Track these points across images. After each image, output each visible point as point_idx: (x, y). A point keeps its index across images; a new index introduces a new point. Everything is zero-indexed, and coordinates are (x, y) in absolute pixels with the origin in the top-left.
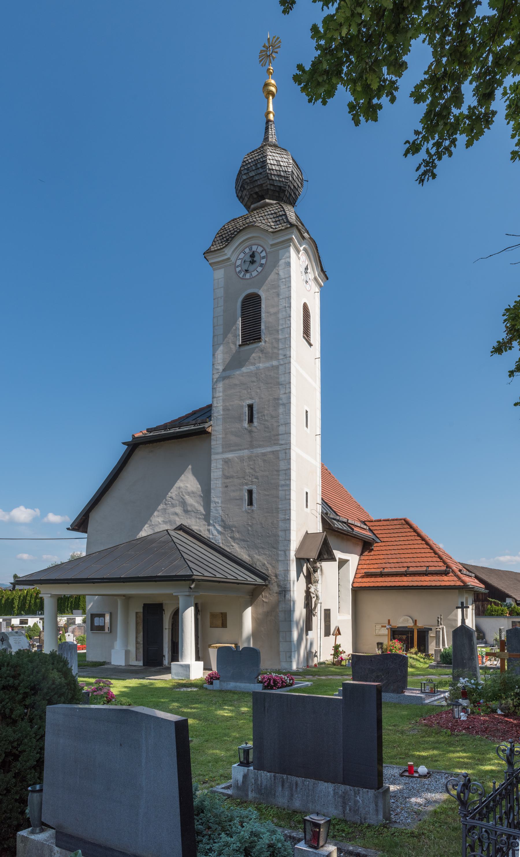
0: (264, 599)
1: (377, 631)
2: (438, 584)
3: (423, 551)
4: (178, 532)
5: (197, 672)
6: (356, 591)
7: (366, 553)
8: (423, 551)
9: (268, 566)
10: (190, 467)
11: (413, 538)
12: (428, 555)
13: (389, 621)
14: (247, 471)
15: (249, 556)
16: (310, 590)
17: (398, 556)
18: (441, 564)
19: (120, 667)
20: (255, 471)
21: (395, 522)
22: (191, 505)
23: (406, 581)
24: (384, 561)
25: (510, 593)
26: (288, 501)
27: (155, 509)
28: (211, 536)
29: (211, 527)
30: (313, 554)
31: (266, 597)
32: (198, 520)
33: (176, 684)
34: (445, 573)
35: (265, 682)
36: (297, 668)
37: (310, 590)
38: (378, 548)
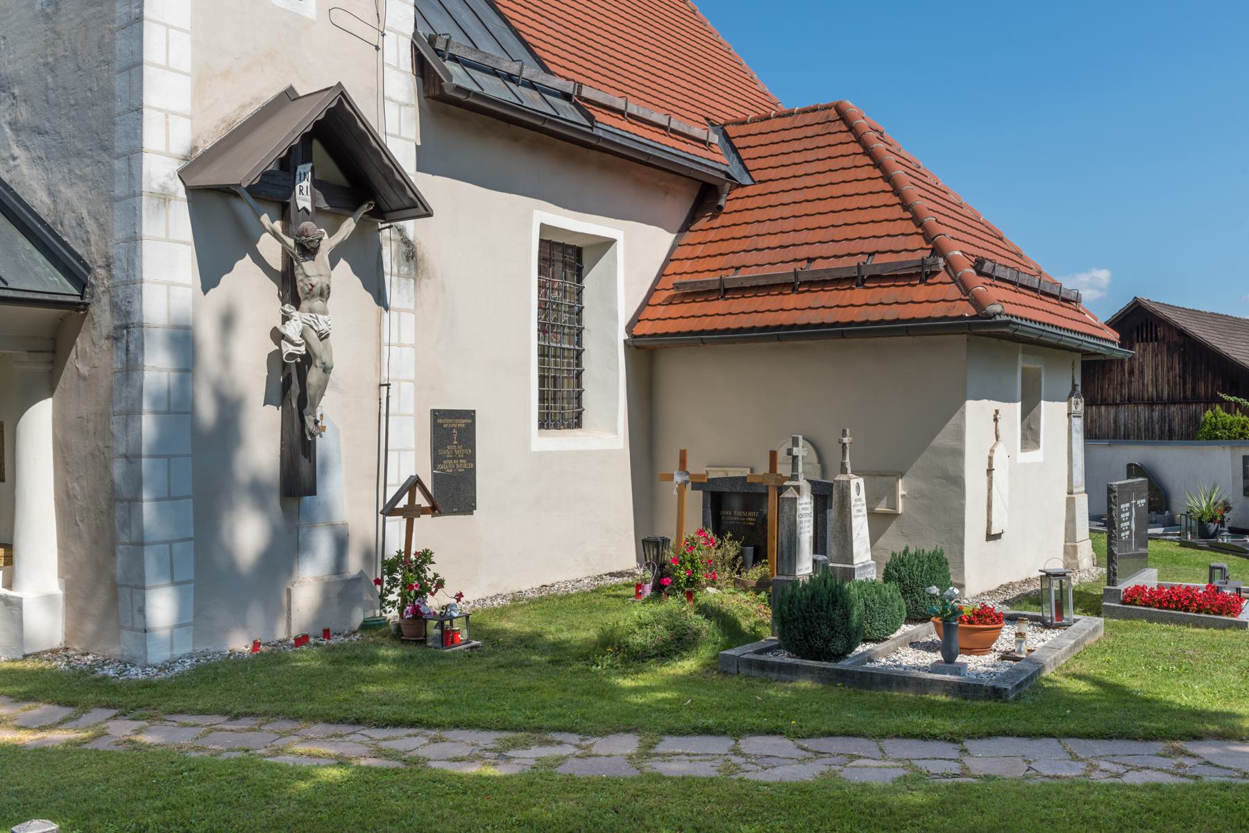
2: (890, 313)
7: (702, 223)
9: (90, 225)
18: (918, 242)
21: (809, 118)
34: (923, 274)
38: (738, 205)
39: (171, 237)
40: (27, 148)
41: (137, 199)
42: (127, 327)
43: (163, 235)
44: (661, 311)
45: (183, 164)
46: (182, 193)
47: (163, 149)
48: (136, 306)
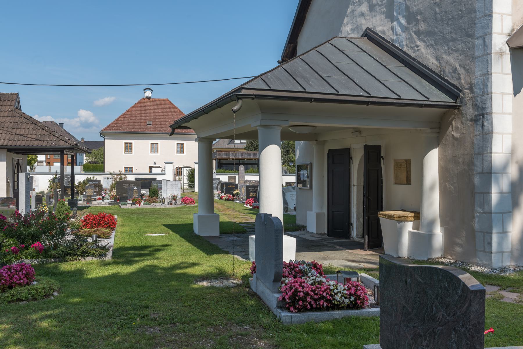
9: (461, 71)
39: (503, 72)
40: (424, 41)
41: (489, 56)
42: (483, 115)
43: (500, 72)
45: (509, 37)
46: (508, 52)
47: (500, 32)
48: (488, 105)
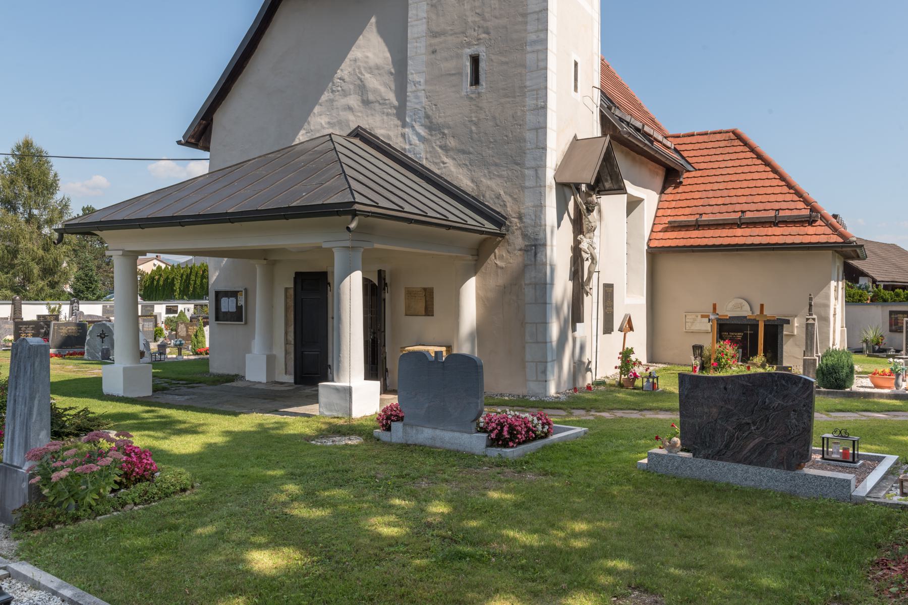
0: (498, 262)
1: (688, 325)
2: (797, 240)
3: (767, 183)
4: (352, 140)
5: (367, 399)
6: (654, 255)
7: (670, 190)
8: (767, 183)
9: (507, 199)
10: (373, 20)
11: (749, 162)
12: (778, 190)
13: (715, 306)
14: (470, 19)
15: (473, 181)
16: (581, 246)
17: (725, 193)
18: (801, 205)
19: (257, 386)
20: (484, 19)
21: (718, 137)
22: (375, 91)
23: (741, 236)
24: (701, 202)
25: (865, 270)
26: (543, 71)
27: (316, 102)
28: (407, 147)
29: (407, 130)
30: (588, 175)
31: (504, 258)
32: (385, 118)
33: (324, 427)
34: (810, 221)
35: (491, 431)
36: (557, 393)
37: (581, 246)
38: (690, 181)
44: (661, 235)
